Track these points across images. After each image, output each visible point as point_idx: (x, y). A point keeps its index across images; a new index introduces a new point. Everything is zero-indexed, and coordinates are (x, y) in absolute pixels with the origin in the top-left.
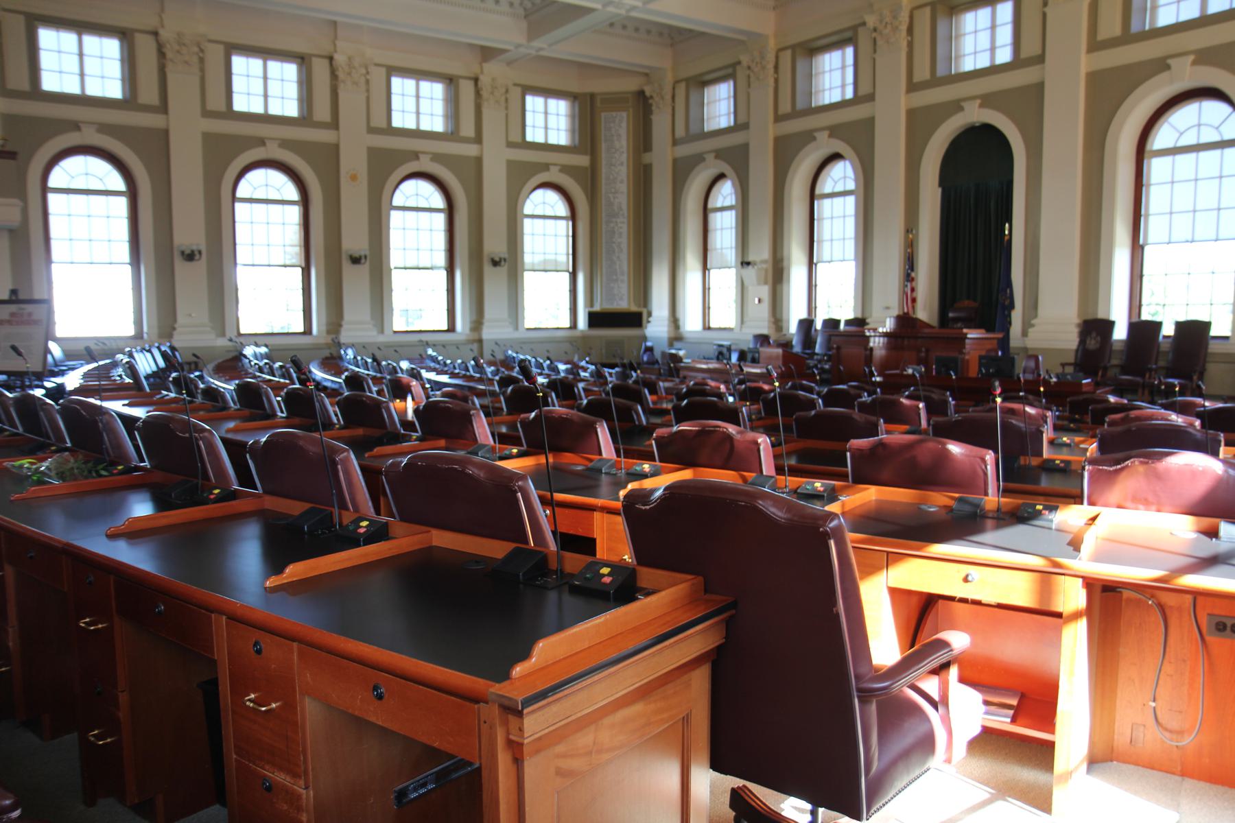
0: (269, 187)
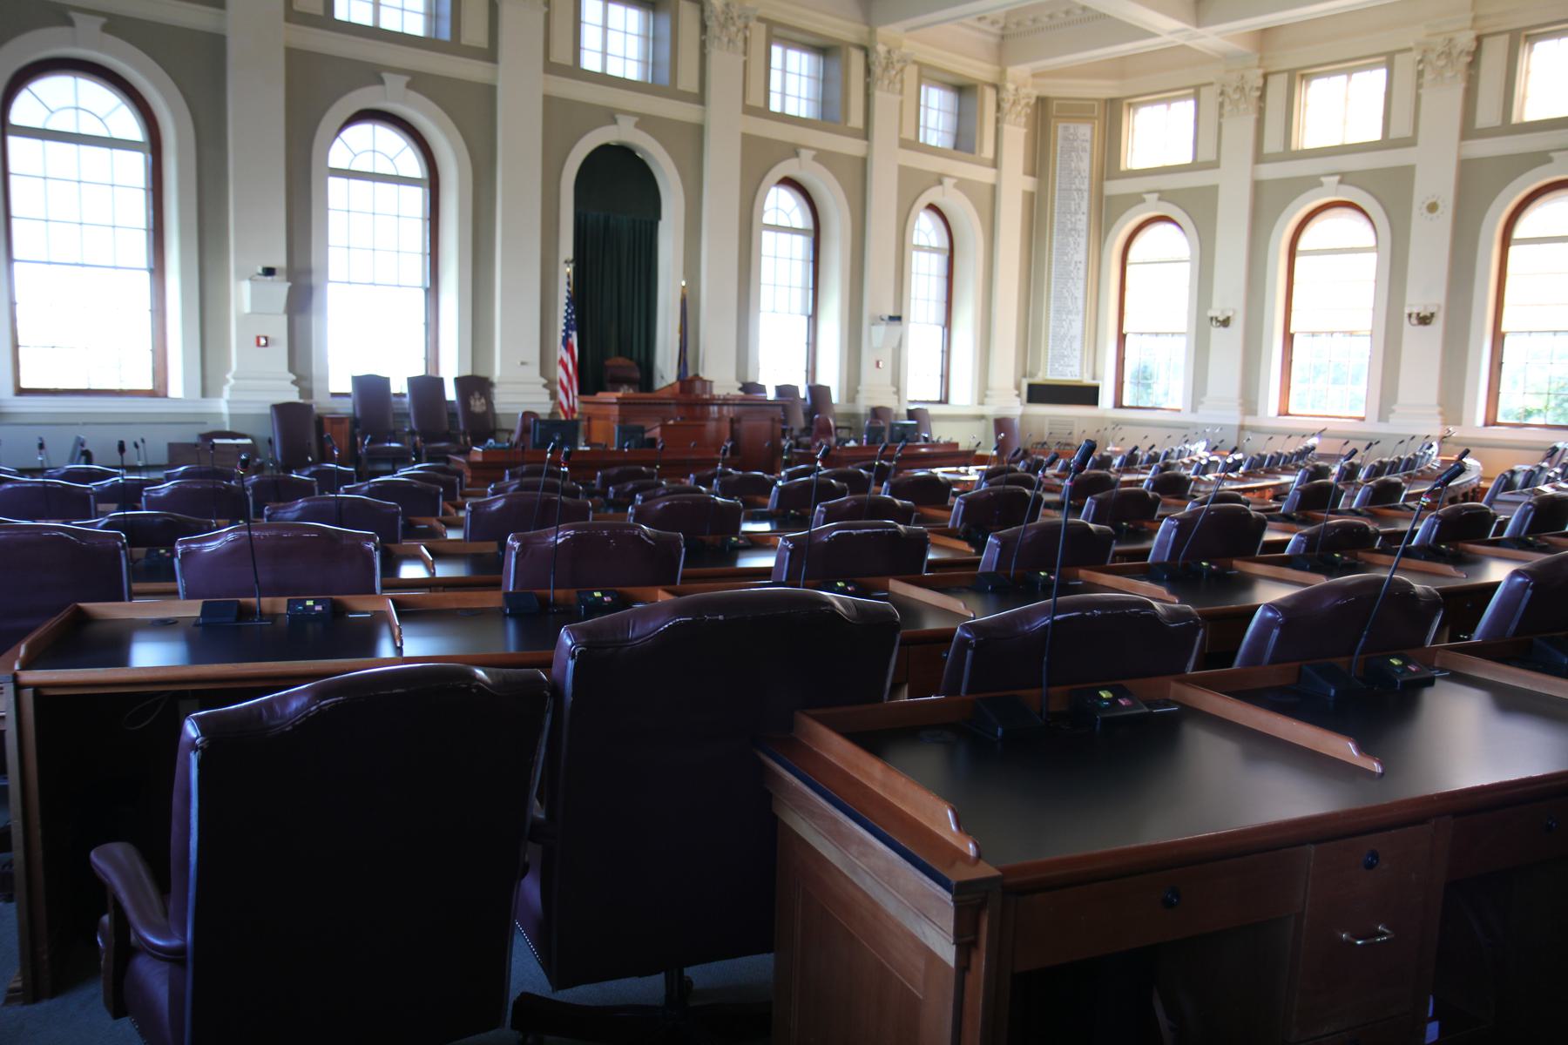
0: (779, 211)
